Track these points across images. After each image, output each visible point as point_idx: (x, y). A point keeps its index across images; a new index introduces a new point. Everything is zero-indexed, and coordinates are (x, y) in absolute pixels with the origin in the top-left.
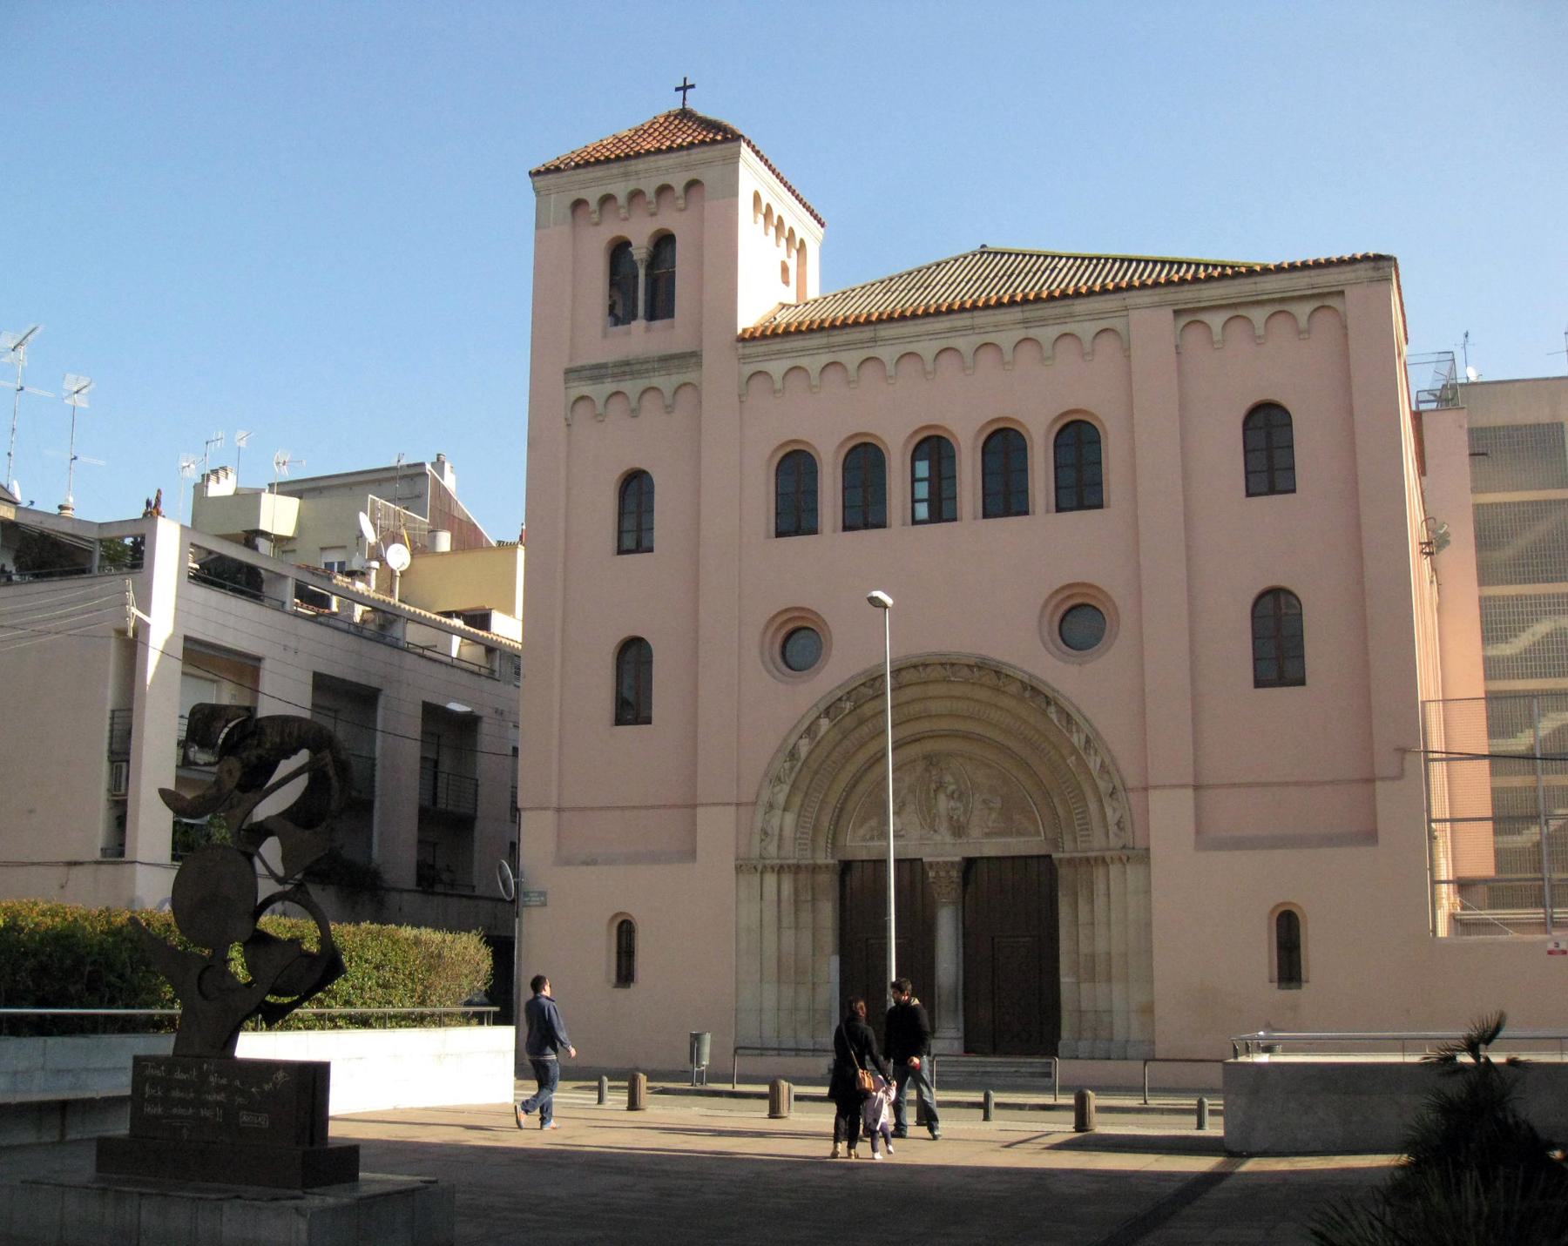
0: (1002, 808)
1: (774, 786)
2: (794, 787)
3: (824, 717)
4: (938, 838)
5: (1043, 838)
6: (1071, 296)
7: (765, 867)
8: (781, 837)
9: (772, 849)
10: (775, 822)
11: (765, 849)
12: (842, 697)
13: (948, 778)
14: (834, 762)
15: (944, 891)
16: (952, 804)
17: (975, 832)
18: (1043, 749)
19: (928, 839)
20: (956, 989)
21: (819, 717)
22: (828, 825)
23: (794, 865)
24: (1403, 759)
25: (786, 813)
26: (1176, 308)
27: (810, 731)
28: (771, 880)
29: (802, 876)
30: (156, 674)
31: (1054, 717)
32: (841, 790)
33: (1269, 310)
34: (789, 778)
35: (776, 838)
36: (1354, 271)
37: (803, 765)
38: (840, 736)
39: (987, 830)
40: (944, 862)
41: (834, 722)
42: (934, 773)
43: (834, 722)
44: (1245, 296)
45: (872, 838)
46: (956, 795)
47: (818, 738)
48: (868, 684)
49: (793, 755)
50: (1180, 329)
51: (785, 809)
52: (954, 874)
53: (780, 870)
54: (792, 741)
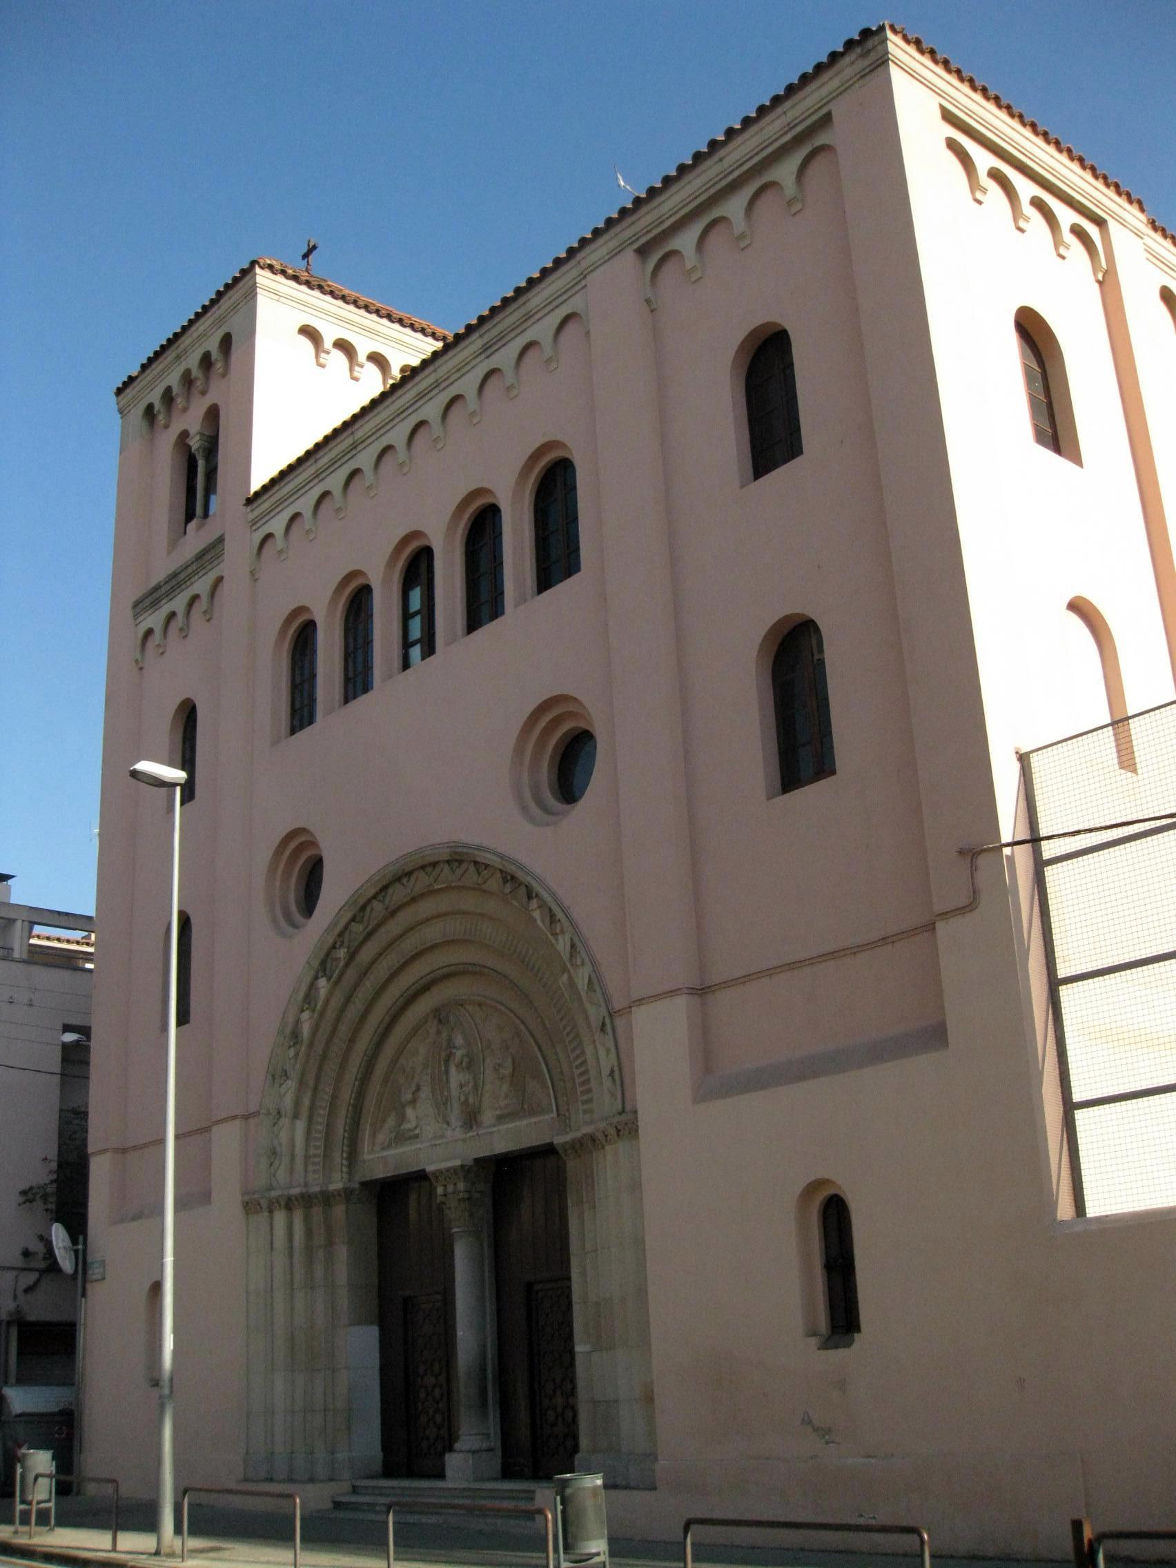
0: (513, 1075)
1: (281, 1085)
2: (302, 1083)
5: (554, 1115)
6: (741, 129)
9: (282, 1175)
10: (284, 1136)
13: (459, 1040)
17: (488, 1116)
18: (533, 967)
20: (483, 1369)
24: (973, 869)
26: (635, 246)
27: (309, 997)
28: (280, 1217)
29: (317, 1213)
30: (176, 1352)
31: (537, 915)
33: (695, 230)
36: (836, 74)
44: (737, 168)
49: (295, 1036)
50: (649, 275)
51: (296, 1116)
53: (289, 1205)
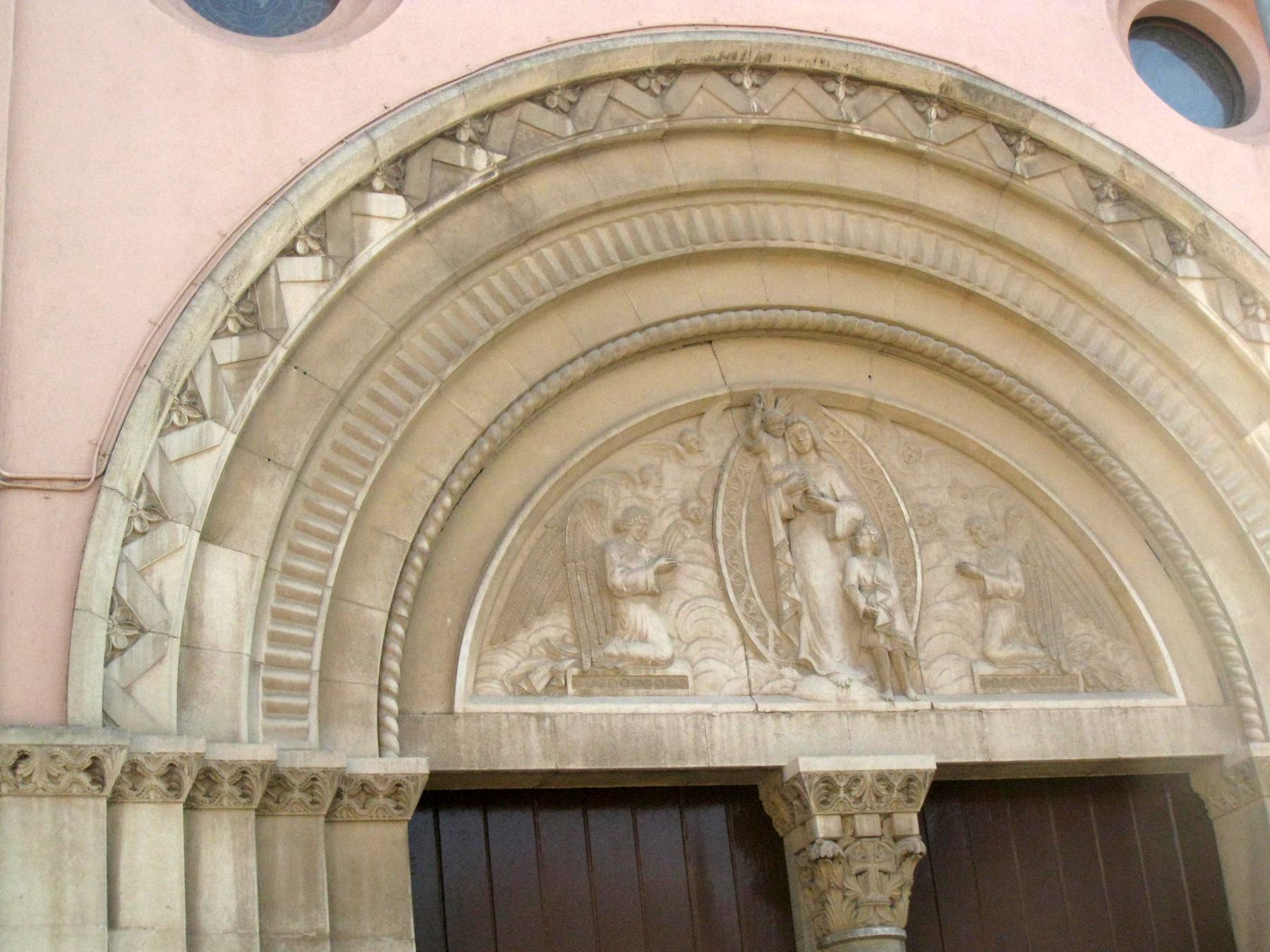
1: (169, 428)
3: (386, 190)
4: (821, 689)
7: (133, 770)
8: (190, 647)
11: (128, 690)
12: (456, 127)
14: (409, 372)
15: (875, 895)
16: (858, 569)
19: (784, 696)
21: (364, 186)
22: (381, 617)
23: (263, 766)
25: (212, 548)
32: (435, 485)
34: (236, 405)
35: (174, 647)
37: (288, 361)
38: (442, 277)
39: (985, 669)
40: (882, 777)
41: (424, 214)
42: (775, 458)
43: (424, 214)
45: (555, 688)
46: (865, 541)
47: (362, 260)
48: (554, 100)
52: (909, 822)
54: (261, 251)
